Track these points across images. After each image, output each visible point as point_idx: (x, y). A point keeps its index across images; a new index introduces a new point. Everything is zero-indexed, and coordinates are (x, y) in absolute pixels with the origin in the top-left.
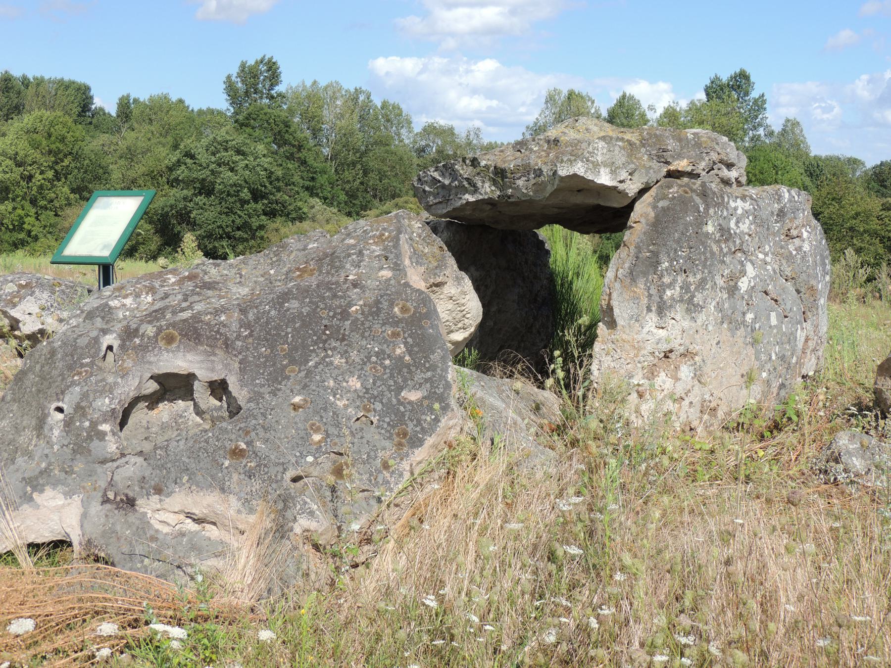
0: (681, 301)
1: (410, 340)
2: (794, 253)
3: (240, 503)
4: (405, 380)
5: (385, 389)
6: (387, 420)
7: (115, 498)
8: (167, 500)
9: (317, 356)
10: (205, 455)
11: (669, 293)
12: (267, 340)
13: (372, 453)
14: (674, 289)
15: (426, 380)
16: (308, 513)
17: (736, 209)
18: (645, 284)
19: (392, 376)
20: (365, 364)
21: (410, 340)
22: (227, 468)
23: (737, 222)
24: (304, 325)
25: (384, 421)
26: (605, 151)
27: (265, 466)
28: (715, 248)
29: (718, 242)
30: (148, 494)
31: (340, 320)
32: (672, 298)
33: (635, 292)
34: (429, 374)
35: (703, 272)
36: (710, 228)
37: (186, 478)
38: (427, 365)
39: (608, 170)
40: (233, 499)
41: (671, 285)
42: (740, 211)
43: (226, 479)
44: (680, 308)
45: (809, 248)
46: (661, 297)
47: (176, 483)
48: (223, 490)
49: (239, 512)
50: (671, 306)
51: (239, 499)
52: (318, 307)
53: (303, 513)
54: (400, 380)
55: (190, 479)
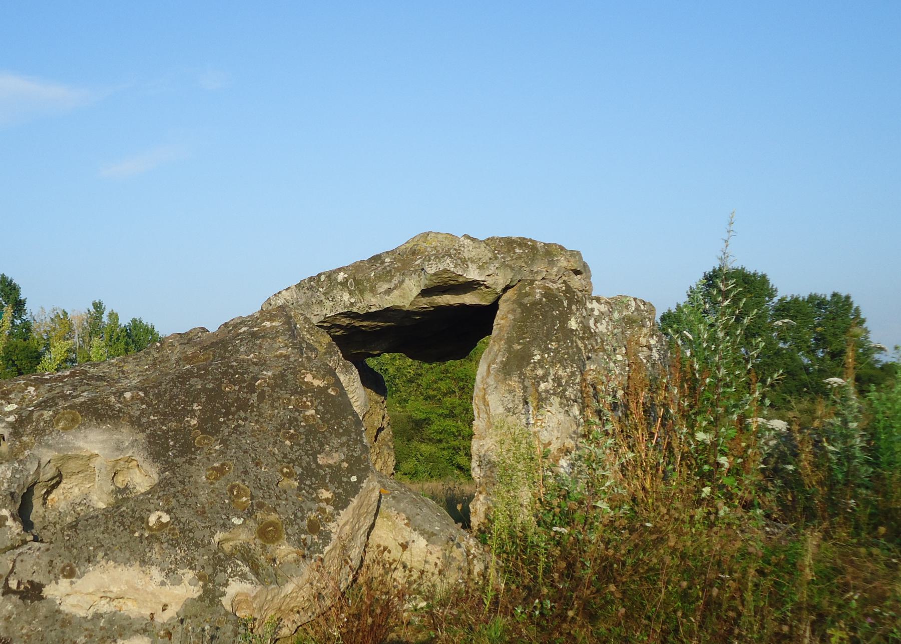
0: (554, 394)
1: (320, 408)
2: (645, 361)
3: (164, 574)
4: (322, 445)
5: (303, 453)
6: (308, 483)
7: (18, 587)
8: (79, 581)
9: (228, 427)
10: (122, 528)
11: (543, 386)
12: (175, 416)
13: (299, 514)
14: (547, 381)
15: (342, 445)
16: (240, 576)
17: (592, 310)
18: (520, 377)
19: (307, 441)
20: (279, 430)
21: (320, 408)
22: (147, 538)
23: (596, 322)
24: (210, 399)
25: (305, 484)
26: (471, 248)
27: (190, 531)
28: (580, 345)
29: (582, 338)
30: (56, 579)
31: (247, 393)
32: (547, 391)
33: (509, 385)
34: (344, 439)
35: (572, 366)
36: (573, 324)
37: (101, 554)
38: (341, 431)
39: (475, 266)
40: (155, 571)
41: (544, 378)
42: (596, 313)
43: (147, 550)
44: (555, 400)
45: (658, 357)
46: (537, 390)
47: (89, 562)
48: (143, 562)
49: (163, 584)
50: (546, 398)
51: (163, 570)
52: (222, 382)
53: (235, 576)
54: (316, 445)
55: (106, 554)
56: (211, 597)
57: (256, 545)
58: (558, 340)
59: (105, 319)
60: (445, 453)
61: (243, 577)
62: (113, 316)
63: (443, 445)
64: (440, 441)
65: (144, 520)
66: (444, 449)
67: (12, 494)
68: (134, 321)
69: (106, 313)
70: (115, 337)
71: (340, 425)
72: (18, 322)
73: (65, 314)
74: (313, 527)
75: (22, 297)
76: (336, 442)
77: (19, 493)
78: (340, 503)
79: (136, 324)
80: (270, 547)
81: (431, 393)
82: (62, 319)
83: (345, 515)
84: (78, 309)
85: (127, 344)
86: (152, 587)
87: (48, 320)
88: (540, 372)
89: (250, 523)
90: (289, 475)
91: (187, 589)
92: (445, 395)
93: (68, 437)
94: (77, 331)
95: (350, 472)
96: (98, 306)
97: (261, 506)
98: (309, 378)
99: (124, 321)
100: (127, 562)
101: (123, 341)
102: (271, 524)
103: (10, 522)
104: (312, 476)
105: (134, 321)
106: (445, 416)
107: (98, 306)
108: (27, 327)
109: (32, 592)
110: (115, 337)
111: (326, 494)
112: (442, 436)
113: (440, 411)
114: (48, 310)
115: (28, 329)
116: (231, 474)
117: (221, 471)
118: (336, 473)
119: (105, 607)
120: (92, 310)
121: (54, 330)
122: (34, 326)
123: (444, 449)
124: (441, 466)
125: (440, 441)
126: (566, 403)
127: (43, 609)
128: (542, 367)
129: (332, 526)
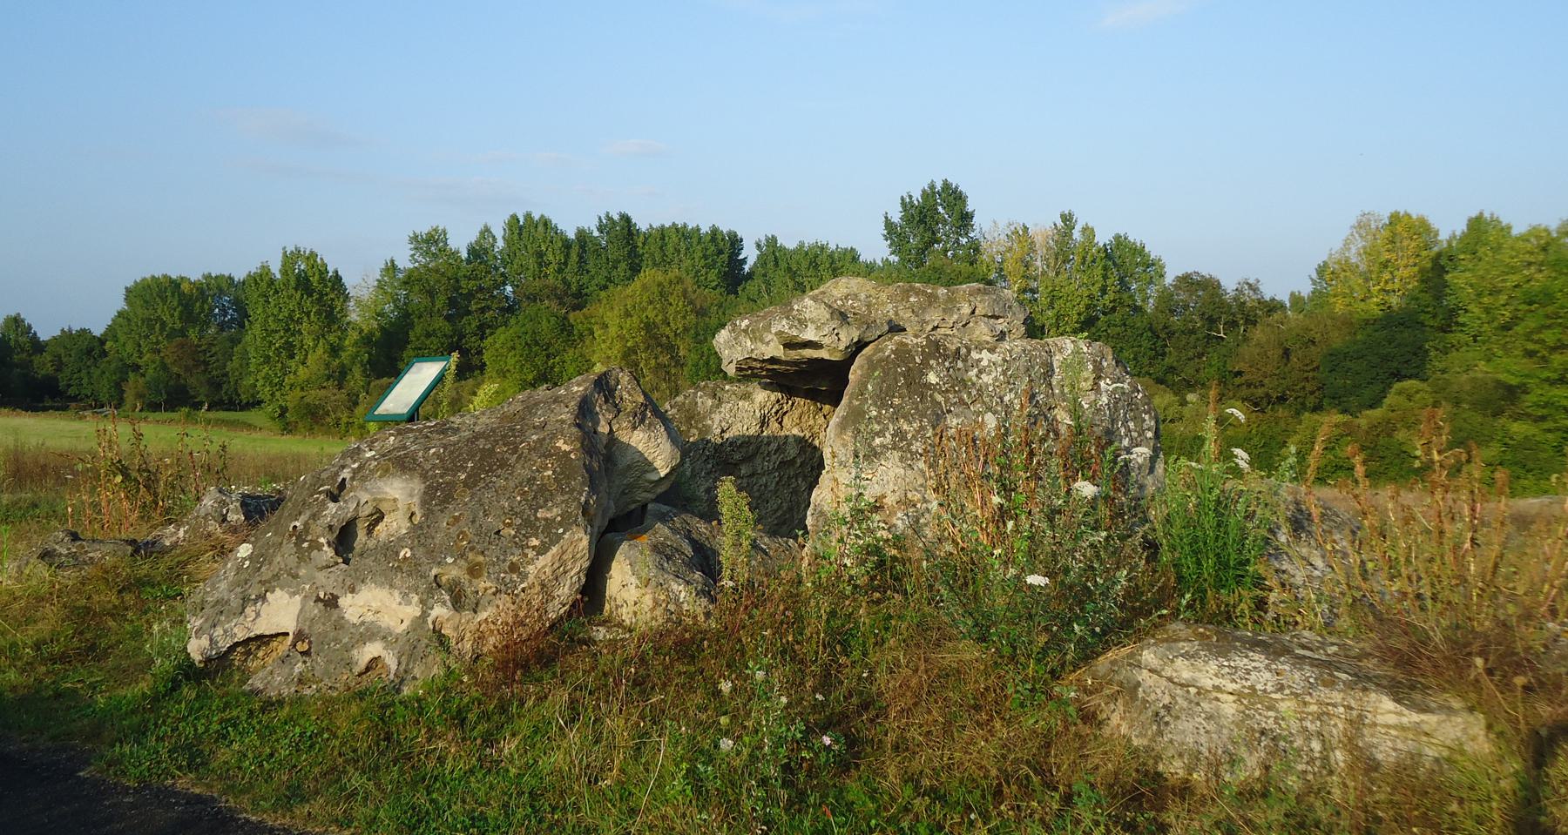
4: (546, 501)
19: (535, 497)
40: (396, 593)
48: (391, 586)
56: (424, 615)
57: (465, 578)
58: (901, 397)
59: (1077, 234)
60: (1550, 436)
61: (444, 603)
62: (1088, 232)
63: (1546, 425)
64: (1543, 418)
65: (397, 554)
66: (1549, 431)
67: (330, 527)
68: (1117, 237)
69: (1078, 228)
70: (1089, 259)
71: (568, 485)
72: (964, 241)
73: (1026, 229)
74: (514, 568)
75: (969, 209)
76: (559, 498)
77: (337, 526)
78: (541, 550)
79: (1120, 241)
80: (475, 581)
81: (1531, 346)
82: (1022, 235)
83: (543, 561)
84: (1042, 223)
85: (1105, 268)
86: (394, 606)
87: (1003, 237)
88: (877, 427)
89: (462, 562)
90: (509, 525)
91: (414, 610)
92: (1553, 349)
93: (380, 484)
94: (1041, 251)
95: (560, 524)
96: (1067, 219)
97: (472, 549)
98: (560, 443)
99: (1103, 238)
100: (382, 585)
101: (1100, 265)
102: (479, 564)
103: (326, 548)
104: (529, 526)
105: (1117, 237)
106: (1552, 383)
107: (1067, 219)
108: (975, 247)
109: (331, 602)
110: (1089, 259)
111: (535, 542)
112: (1545, 412)
113: (1546, 374)
114: (1002, 224)
115: (977, 250)
116: (462, 523)
117: (457, 519)
118: (549, 523)
119: (369, 617)
120: (1060, 224)
121: (1010, 249)
122: (984, 245)
123: (1549, 431)
124: (1542, 455)
125: (1543, 418)
126: (908, 458)
127: (335, 614)
128: (879, 423)
129: (531, 569)
